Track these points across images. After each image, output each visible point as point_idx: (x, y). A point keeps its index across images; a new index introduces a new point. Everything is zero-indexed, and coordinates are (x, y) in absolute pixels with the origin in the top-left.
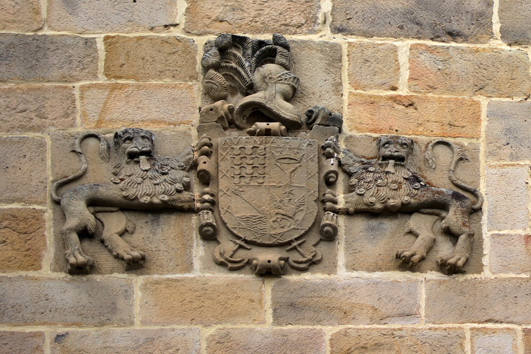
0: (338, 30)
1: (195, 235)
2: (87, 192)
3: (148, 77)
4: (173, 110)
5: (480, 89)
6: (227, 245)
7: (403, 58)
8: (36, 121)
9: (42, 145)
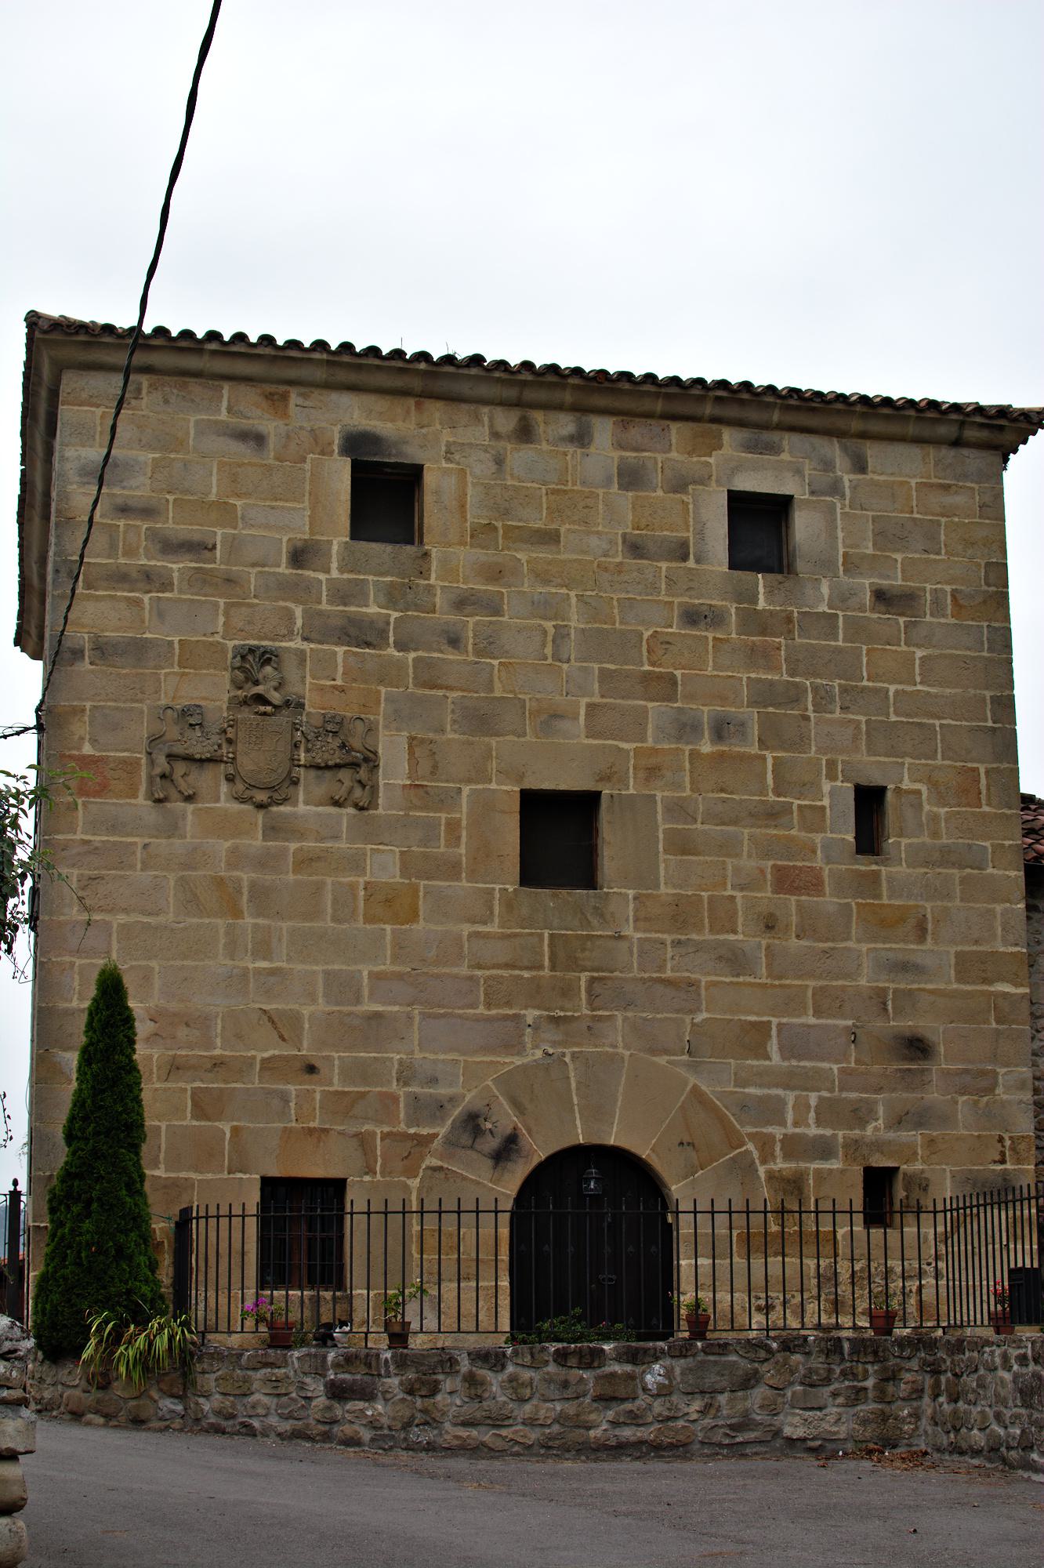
0: (305, 639)
1: (222, 777)
2: (166, 750)
3: (201, 668)
4: (213, 691)
5: (381, 682)
6: (240, 786)
7: (340, 659)
8: (140, 696)
9: (142, 712)
